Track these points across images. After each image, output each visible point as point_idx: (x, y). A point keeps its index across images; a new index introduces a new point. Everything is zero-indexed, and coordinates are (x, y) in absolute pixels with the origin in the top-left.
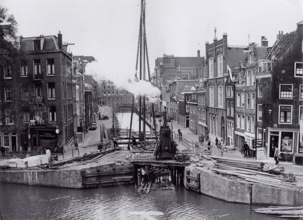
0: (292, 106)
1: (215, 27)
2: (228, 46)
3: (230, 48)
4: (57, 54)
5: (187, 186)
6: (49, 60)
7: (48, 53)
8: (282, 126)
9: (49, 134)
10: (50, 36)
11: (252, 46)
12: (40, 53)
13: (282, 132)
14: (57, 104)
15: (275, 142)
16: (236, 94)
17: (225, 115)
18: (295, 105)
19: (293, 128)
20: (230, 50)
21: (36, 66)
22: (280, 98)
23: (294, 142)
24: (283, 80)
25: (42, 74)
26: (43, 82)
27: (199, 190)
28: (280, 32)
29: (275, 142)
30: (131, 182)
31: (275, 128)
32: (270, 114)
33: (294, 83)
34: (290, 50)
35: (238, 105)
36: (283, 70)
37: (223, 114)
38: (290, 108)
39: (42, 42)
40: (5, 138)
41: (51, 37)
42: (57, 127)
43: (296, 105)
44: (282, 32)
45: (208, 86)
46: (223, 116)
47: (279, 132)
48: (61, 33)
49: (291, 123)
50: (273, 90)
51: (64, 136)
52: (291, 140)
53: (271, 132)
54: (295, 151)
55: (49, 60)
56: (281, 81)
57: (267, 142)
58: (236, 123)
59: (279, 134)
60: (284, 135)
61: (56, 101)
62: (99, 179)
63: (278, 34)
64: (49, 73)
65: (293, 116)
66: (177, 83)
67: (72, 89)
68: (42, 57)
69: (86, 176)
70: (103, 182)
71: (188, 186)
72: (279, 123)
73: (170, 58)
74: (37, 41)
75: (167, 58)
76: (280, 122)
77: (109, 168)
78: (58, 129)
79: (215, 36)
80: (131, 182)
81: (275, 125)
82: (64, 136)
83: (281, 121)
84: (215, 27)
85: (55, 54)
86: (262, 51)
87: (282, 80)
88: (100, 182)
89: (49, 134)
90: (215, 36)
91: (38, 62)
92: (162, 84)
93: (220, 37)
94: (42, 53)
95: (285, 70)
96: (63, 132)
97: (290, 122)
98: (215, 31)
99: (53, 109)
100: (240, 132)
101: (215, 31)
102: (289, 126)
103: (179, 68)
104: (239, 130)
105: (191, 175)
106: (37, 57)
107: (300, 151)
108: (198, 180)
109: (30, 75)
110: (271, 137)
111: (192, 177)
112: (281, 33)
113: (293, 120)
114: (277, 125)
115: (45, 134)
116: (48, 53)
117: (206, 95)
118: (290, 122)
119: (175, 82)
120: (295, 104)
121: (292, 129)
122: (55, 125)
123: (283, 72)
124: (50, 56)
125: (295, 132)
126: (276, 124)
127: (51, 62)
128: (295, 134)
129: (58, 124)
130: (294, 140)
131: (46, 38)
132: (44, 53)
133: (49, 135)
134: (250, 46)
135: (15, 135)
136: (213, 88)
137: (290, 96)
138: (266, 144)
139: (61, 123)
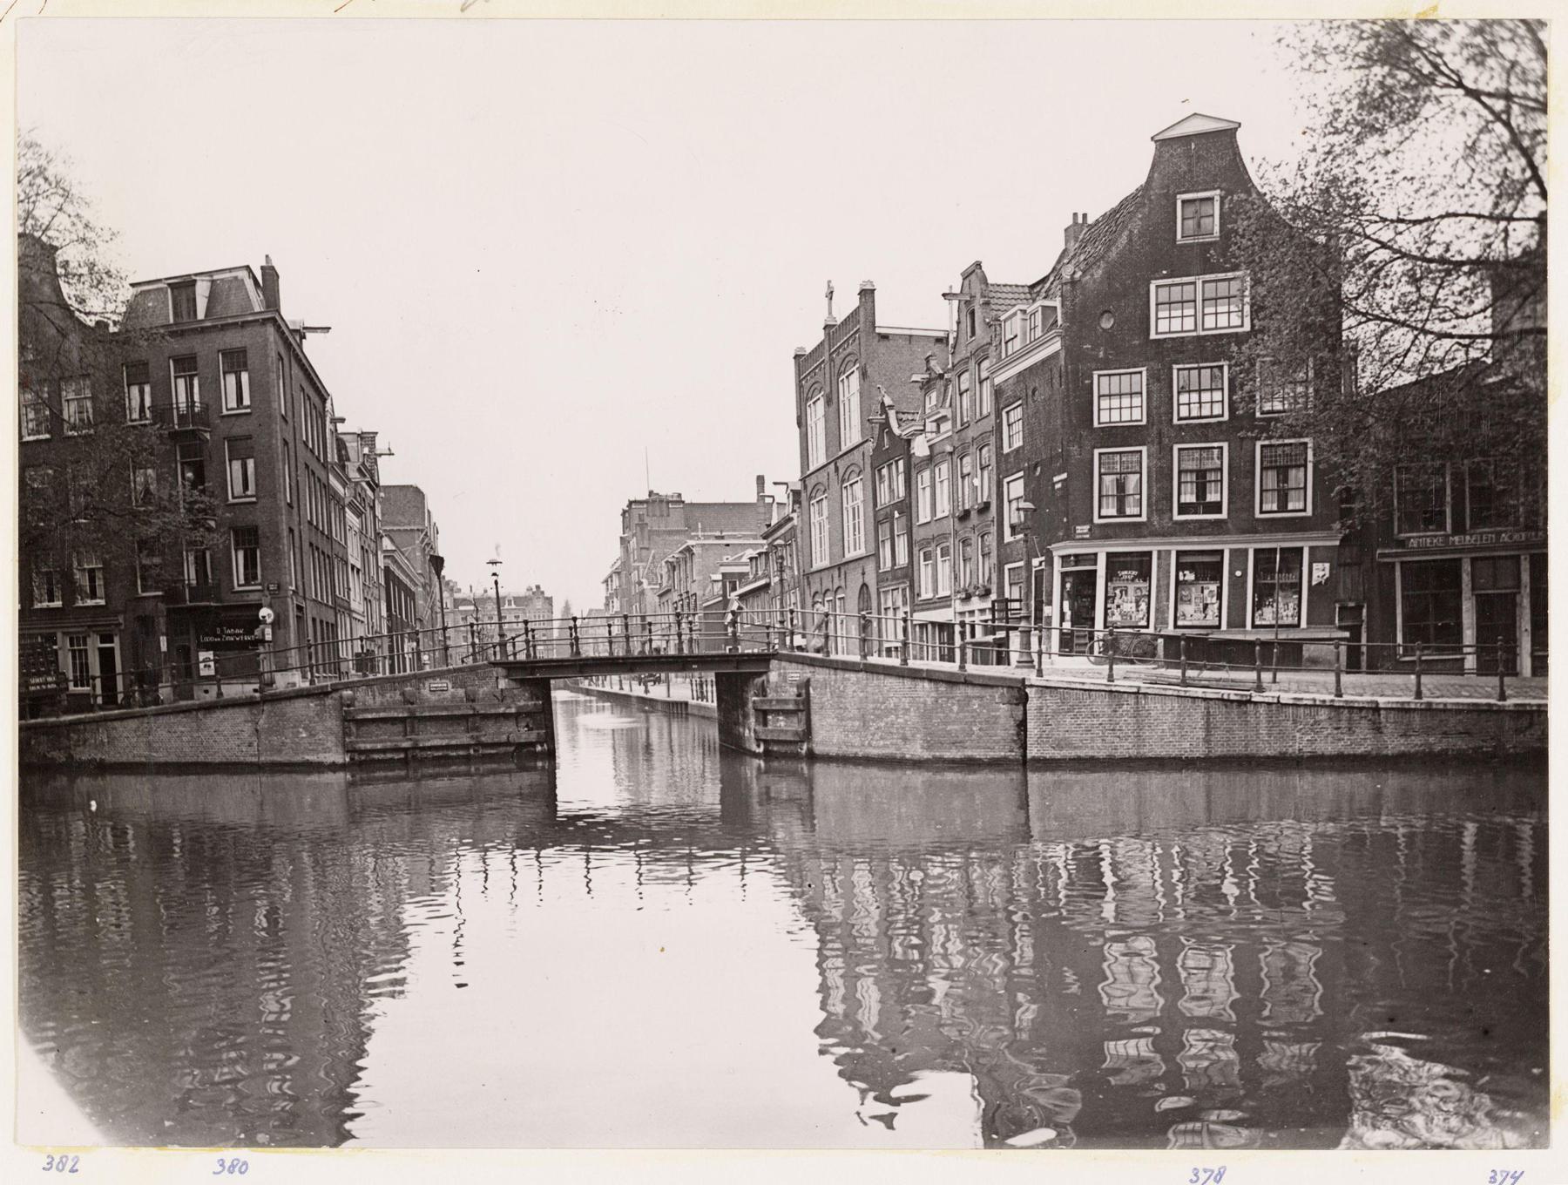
0: (1144, 449)
1: (829, 282)
2: (878, 330)
3: (885, 337)
4: (257, 329)
5: (758, 740)
6: (226, 353)
7: (224, 327)
8: (1106, 532)
9: (237, 631)
10: (230, 270)
11: (973, 277)
12: (194, 331)
13: (1109, 555)
14: (260, 518)
15: (1081, 587)
16: (913, 482)
17: (874, 576)
18: (1156, 447)
19: (1154, 534)
20: (886, 342)
21: (181, 382)
22: (1096, 424)
23: (1158, 586)
24: (1105, 353)
25: (206, 407)
26: (208, 436)
27: (805, 747)
28: (1075, 215)
29: (1081, 587)
30: (539, 748)
31: (1083, 539)
32: (1058, 494)
33: (1152, 363)
34: (1130, 240)
35: (924, 515)
36: (1106, 315)
37: (863, 574)
38: (1135, 458)
39: (202, 290)
40: (74, 658)
41: (234, 274)
42: (267, 600)
43: (1160, 443)
44: (1085, 216)
45: (805, 503)
46: (866, 581)
47: (1096, 555)
48: (275, 263)
49: (1144, 518)
50: (1068, 396)
51: (292, 636)
52: (1144, 585)
53: (1065, 558)
54: (1161, 620)
55: (226, 353)
56: (1096, 359)
57: (1050, 603)
58: (916, 585)
59: (1095, 564)
60: (1116, 563)
61: (258, 506)
62: (412, 732)
63: (1070, 222)
64: (233, 403)
65: (1149, 487)
66: (694, 550)
67: (332, 573)
68: (197, 345)
69: (360, 717)
70: (428, 744)
71: (763, 737)
72: (1097, 520)
73: (668, 502)
74: (183, 287)
75: (661, 501)
76: (1100, 517)
77: (451, 690)
78: (270, 606)
79: (830, 313)
80: (539, 748)
81: (1083, 529)
82: (292, 636)
83: (1104, 513)
84: (829, 282)
85: (248, 331)
86: (1011, 296)
87: (1101, 354)
88: (416, 741)
89: (237, 631)
90: (830, 313)
91: (187, 365)
92: (645, 581)
93: (846, 304)
94: (204, 330)
95: (1114, 316)
96: (287, 617)
97: (1140, 516)
98: (830, 295)
99: (249, 538)
100: (935, 608)
101: (830, 295)
102: (1136, 530)
103: (700, 534)
104: (929, 605)
105: (771, 695)
106: (179, 346)
107: (1180, 623)
108: (801, 707)
109: (162, 411)
110: (1064, 575)
111: (778, 701)
112: (1080, 220)
113: (1149, 505)
114: (1090, 530)
115: (222, 631)
116: (224, 327)
117: (799, 535)
118: (1140, 516)
119: (688, 549)
120: (1156, 441)
121: (1148, 540)
122: (253, 597)
123: (1107, 323)
124: (233, 339)
125: (1159, 552)
126: (1084, 524)
127: (236, 360)
128: (1159, 558)
129: (267, 593)
130: (1158, 580)
131: (215, 277)
132: (207, 327)
133: (238, 635)
134: (967, 282)
135: (112, 642)
136: (825, 503)
137: (1137, 414)
138: (1047, 610)
139: (279, 587)
